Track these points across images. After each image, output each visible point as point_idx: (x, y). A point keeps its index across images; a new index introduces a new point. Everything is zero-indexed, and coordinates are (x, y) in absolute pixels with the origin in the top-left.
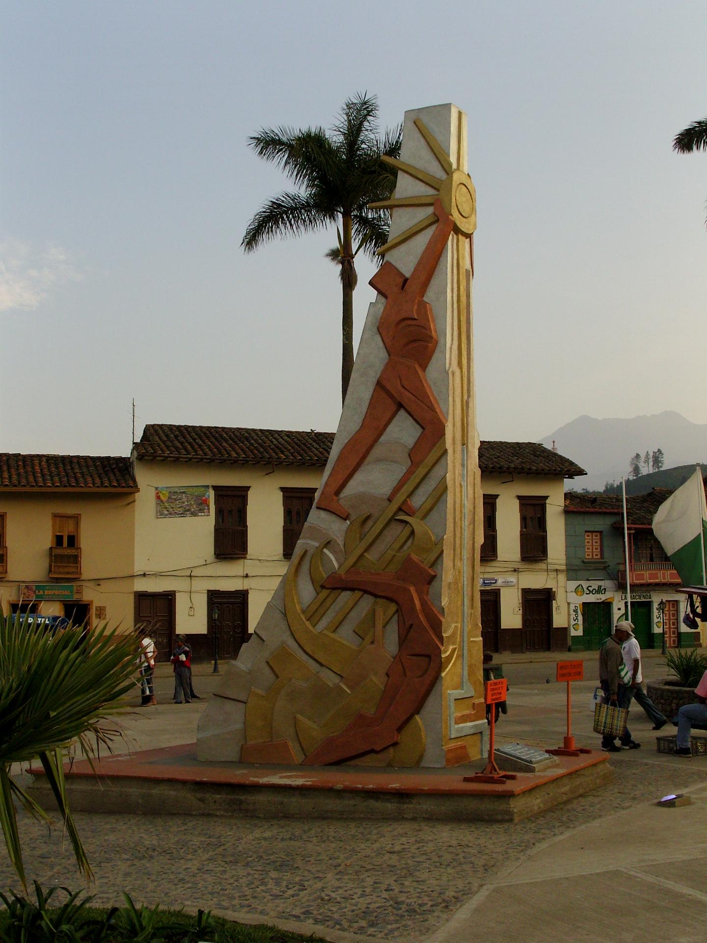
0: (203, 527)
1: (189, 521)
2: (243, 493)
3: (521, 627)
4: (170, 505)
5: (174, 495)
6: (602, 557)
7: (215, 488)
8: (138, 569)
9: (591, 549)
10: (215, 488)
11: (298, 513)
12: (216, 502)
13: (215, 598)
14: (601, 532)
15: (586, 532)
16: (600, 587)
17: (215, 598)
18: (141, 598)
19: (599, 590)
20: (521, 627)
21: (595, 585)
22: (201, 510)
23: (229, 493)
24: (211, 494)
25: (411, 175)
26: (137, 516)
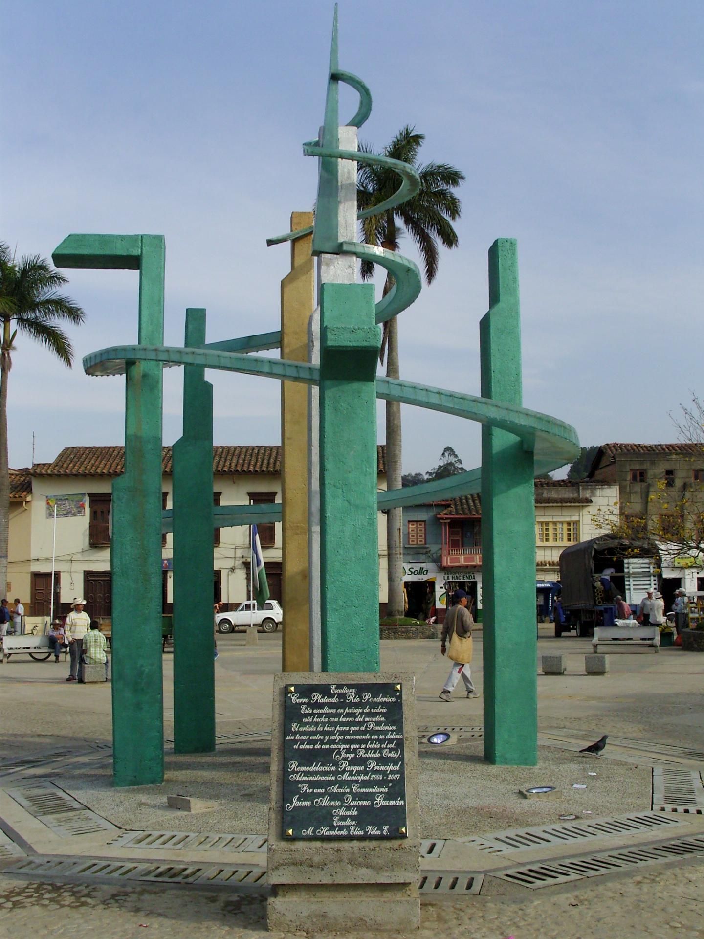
0: (82, 522)
1: (71, 520)
2: (271, 498)
3: (216, 443)
4: (64, 508)
5: (59, 500)
6: (425, 544)
7: (89, 495)
8: (34, 555)
9: (417, 539)
10: (89, 495)
11: (102, 512)
12: (91, 507)
13: (89, 576)
14: (425, 521)
15: (409, 522)
16: (422, 569)
17: (89, 576)
18: (36, 576)
19: (421, 571)
20: (216, 443)
21: (417, 567)
22: (80, 512)
23: (263, 498)
24: (87, 502)
25: (140, 302)
26: (33, 517)
